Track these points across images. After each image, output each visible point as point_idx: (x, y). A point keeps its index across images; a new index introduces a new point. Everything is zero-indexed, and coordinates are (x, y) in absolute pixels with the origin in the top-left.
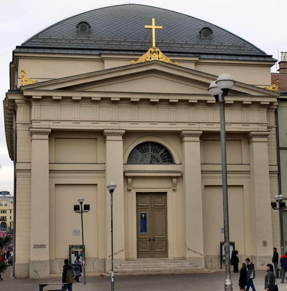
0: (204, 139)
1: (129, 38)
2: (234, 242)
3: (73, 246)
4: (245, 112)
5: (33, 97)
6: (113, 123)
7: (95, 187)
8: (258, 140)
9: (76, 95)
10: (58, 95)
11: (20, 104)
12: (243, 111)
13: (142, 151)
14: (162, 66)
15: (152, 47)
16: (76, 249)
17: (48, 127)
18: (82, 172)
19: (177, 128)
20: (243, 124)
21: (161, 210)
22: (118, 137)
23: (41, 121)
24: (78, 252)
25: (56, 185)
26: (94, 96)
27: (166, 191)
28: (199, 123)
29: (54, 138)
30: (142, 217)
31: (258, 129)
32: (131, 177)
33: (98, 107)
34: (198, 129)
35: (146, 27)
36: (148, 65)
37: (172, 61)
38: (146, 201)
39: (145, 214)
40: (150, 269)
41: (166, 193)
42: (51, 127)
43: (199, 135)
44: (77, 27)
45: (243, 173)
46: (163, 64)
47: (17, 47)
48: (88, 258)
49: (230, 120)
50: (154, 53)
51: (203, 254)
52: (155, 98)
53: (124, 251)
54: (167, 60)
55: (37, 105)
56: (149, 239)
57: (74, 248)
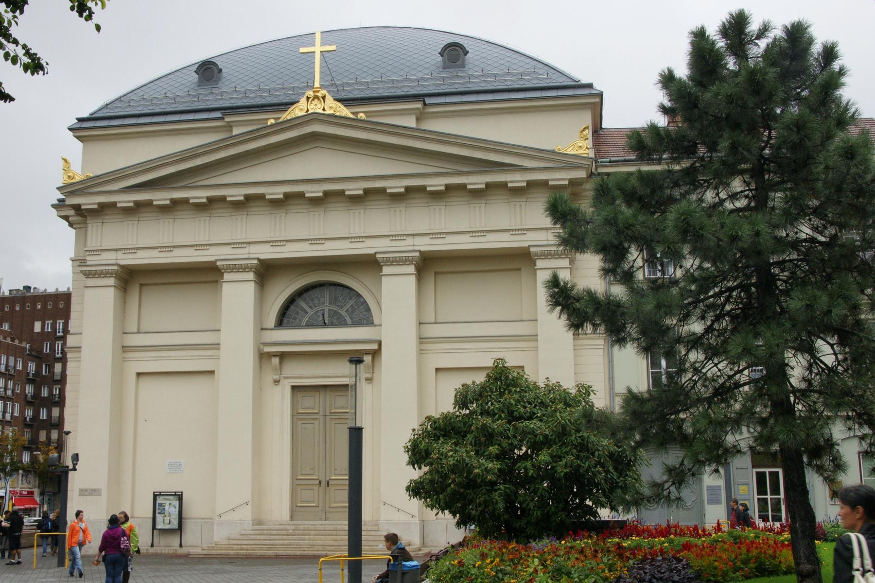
0: (438, 270)
1: (386, 72)
3: (160, 492)
6: (394, 238)
9: (161, 197)
10: (126, 200)
12: (472, 206)
15: (313, 88)
17: (411, 248)
18: (444, 340)
19: (491, 243)
20: (512, 233)
21: (312, 422)
22: (232, 274)
23: (102, 253)
26: (231, 194)
28: (413, 235)
29: (433, 274)
31: (548, 240)
32: (278, 354)
33: (484, 205)
35: (302, 50)
36: (301, 124)
37: (368, 114)
42: (417, 248)
43: (251, 268)
44: (441, 54)
45: (443, 342)
46: (333, 120)
47: (80, 120)
48: (188, 517)
49: (483, 225)
50: (316, 100)
51: (417, 515)
52: (313, 190)
53: (250, 504)
54: (344, 111)
55: (95, 221)
56: (317, 482)
57: (162, 497)
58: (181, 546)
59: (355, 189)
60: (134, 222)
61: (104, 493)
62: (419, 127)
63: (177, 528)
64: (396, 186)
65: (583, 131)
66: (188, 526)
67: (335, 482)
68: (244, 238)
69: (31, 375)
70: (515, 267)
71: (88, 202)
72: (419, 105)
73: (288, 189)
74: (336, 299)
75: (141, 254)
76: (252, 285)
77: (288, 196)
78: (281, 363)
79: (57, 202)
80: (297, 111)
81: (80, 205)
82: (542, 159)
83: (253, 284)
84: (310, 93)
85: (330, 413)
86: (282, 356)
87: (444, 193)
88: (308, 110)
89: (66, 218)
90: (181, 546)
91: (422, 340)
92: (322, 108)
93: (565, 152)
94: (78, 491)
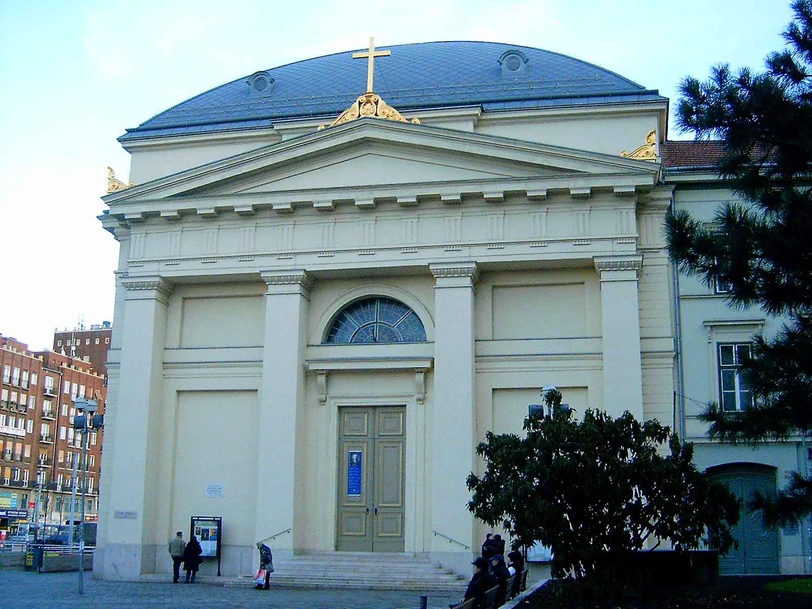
2: (221, 518)
4: (537, 218)
5: (572, 192)
7: (583, 392)
8: (279, 290)
9: (205, 205)
10: (170, 209)
11: (123, 236)
13: (386, 314)
14: (381, 127)
16: (204, 525)
24: (208, 530)
25: (179, 392)
27: (404, 404)
29: (181, 300)
30: (351, 459)
33: (417, 219)
34: (467, 259)
38: (364, 424)
39: (360, 454)
40: (319, 575)
41: (405, 406)
43: (297, 280)
46: (389, 124)
47: (129, 131)
51: (471, 547)
54: (398, 116)
58: (219, 574)
59: (408, 196)
60: (251, 228)
61: (140, 517)
62: (476, 132)
63: (215, 555)
64: (453, 193)
65: (650, 136)
66: (227, 553)
67: (384, 510)
68: (501, 238)
69: (48, 391)
70: (578, 280)
71: (133, 211)
72: (477, 111)
73: (337, 196)
74: (387, 313)
75: (221, 263)
76: (298, 298)
77: (337, 204)
78: (327, 381)
79: (104, 214)
80: (349, 115)
81: (123, 215)
82: (606, 165)
83: (298, 297)
84: (363, 98)
85: (379, 436)
86: (329, 374)
87: (460, 203)
88: (359, 116)
89: (111, 230)
90: (219, 574)
91: (478, 358)
92: (375, 113)
93: (636, 158)
94: (113, 513)
